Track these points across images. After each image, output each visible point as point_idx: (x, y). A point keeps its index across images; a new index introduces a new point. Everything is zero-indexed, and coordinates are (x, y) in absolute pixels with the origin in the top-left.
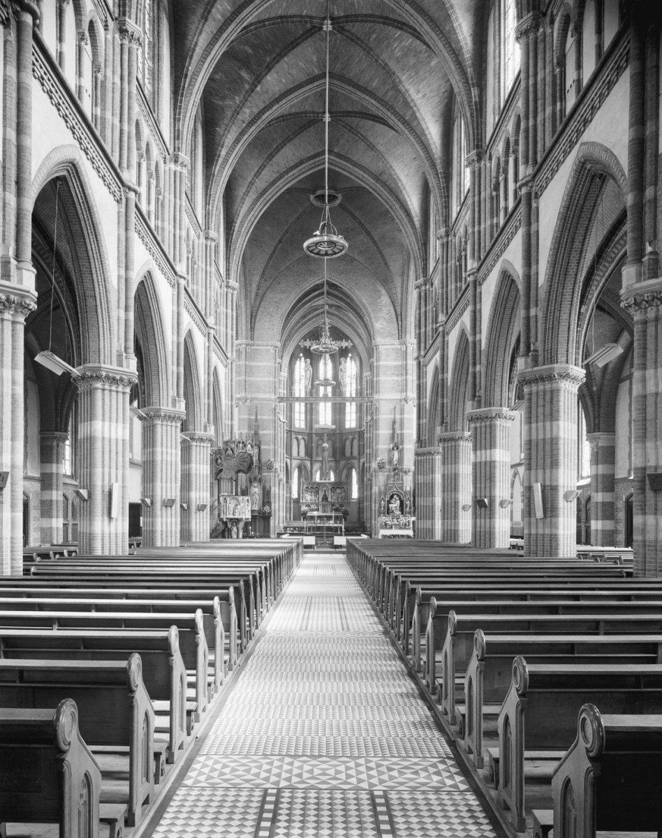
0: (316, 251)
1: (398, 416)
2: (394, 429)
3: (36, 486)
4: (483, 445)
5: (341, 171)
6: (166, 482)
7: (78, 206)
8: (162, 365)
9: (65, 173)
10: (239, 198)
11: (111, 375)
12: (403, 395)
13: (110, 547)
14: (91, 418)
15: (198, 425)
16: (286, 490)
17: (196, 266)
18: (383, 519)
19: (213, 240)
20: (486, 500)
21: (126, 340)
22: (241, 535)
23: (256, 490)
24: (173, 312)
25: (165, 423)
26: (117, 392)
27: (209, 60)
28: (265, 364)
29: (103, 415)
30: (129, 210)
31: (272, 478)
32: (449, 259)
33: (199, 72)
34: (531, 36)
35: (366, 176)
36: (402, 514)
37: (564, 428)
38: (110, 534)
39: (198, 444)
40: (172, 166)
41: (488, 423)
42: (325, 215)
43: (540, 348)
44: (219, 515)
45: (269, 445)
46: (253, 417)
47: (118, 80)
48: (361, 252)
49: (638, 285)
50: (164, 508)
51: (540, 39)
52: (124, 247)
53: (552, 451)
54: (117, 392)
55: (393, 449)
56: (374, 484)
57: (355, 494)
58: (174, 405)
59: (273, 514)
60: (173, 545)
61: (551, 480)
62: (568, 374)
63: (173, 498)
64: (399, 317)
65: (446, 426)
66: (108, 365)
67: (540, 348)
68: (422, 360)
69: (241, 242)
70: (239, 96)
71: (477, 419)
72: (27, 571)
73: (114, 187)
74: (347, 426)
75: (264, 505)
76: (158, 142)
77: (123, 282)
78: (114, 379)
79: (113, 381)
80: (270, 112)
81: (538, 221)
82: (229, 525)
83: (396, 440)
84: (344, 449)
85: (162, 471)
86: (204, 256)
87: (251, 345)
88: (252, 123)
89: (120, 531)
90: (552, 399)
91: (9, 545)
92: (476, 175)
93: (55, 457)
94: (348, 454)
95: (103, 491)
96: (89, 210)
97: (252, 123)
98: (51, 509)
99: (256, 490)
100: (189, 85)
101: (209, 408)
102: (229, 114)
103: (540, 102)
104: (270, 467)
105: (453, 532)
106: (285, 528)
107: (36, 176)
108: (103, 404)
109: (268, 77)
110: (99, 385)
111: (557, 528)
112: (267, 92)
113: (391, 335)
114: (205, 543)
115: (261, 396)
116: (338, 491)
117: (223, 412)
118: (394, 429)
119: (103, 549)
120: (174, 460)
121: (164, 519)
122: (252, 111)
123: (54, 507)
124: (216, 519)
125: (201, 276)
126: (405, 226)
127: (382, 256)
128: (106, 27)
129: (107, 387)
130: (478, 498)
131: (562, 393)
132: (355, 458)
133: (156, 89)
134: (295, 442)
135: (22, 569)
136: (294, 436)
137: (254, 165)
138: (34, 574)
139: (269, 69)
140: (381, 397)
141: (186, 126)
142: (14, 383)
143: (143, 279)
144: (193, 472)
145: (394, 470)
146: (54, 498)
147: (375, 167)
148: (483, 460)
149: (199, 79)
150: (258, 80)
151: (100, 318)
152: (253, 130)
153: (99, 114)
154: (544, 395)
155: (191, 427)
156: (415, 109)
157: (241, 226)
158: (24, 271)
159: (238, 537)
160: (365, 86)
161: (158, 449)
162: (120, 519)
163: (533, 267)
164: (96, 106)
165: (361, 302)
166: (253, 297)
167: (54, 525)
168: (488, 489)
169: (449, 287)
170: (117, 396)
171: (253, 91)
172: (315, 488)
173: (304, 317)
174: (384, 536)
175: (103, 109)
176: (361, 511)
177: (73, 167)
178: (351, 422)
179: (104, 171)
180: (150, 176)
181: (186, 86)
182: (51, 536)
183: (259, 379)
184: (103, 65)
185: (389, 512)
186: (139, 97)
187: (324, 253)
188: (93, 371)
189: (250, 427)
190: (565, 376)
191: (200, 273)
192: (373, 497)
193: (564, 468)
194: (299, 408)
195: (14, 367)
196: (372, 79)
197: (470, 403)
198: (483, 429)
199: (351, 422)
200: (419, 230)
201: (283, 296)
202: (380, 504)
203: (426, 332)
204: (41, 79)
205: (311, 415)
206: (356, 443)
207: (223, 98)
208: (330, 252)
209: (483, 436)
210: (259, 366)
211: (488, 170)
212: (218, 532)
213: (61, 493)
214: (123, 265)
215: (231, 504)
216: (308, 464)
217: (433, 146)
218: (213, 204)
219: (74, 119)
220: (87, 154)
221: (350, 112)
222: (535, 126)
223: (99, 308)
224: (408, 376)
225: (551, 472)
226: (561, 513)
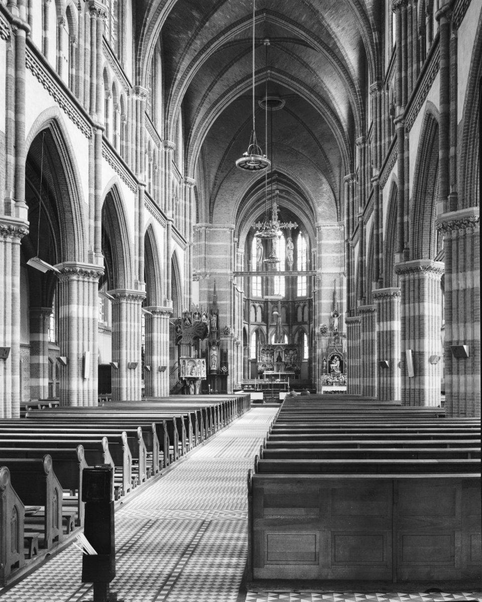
0: (246, 167)
1: (338, 288)
2: (334, 299)
3: (27, 352)
4: (385, 318)
5: (281, 84)
6: (130, 349)
7: (58, 148)
8: (126, 255)
9: (49, 126)
10: (195, 108)
11: (84, 270)
13: (84, 401)
14: (69, 302)
15: (158, 300)
16: (242, 355)
17: (157, 170)
18: (325, 377)
19: (171, 148)
20: (387, 362)
21: (95, 243)
22: (197, 392)
23: (215, 353)
24: (135, 212)
25: (129, 302)
26: (89, 282)
27: (163, 11)
28: (221, 243)
29: (78, 300)
30: (97, 144)
31: (229, 342)
32: (366, 162)
33: (156, 21)
34: (403, 9)
35: (302, 88)
36: (342, 372)
37: (429, 309)
38: (83, 391)
39: (159, 316)
40: (135, 97)
41: (388, 300)
42: (252, 138)
43: (410, 247)
44: (179, 375)
45: (226, 313)
46: (212, 290)
47: (88, 46)
48: (305, 146)
49: (444, 215)
50: (129, 370)
51: (409, 11)
52: (93, 172)
53: (419, 326)
54: (89, 282)
55: (334, 316)
56: (317, 347)
58: (136, 287)
59: (229, 373)
60: (137, 400)
61: (419, 348)
62: (430, 267)
63: (136, 362)
64: (338, 202)
65: (365, 300)
66: (82, 262)
67: (410, 247)
68: (350, 242)
69: (196, 146)
70: (191, 31)
71: (380, 296)
72: (22, 416)
73: (86, 128)
74: (299, 295)
75: (221, 366)
76: (122, 80)
77: (93, 198)
78: (86, 272)
79: (86, 274)
80: (217, 42)
81: (408, 150)
82: (188, 384)
83: (336, 309)
84: (296, 315)
85: (127, 340)
86: (164, 161)
87: (210, 227)
88: (203, 50)
89: (91, 389)
90: (419, 285)
91: (10, 398)
92: (378, 101)
93: (41, 328)
94: (300, 319)
95: (78, 358)
96: (67, 149)
97: (203, 50)
98: (39, 371)
99: (215, 353)
100: (148, 31)
102: (183, 45)
103: (409, 60)
104: (226, 332)
105: (371, 388)
106: (243, 386)
107: (28, 137)
108: (78, 292)
109: (215, 15)
110: (75, 277)
111: (423, 384)
112: (214, 27)
113: (331, 218)
115: (219, 271)
116: (291, 352)
117: (183, 288)
118: (334, 299)
119: (78, 402)
120: (136, 331)
121: (129, 378)
122: (202, 42)
123: (41, 369)
124: (177, 379)
125: (161, 178)
126: (336, 130)
127: (322, 150)
128: (79, 8)
129: (81, 279)
130: (382, 361)
131: (426, 282)
132: (305, 323)
133: (121, 39)
134: (252, 309)
135: (19, 415)
136: (251, 304)
137: (207, 81)
138: (27, 418)
139: (215, 9)
141: (145, 64)
142: (13, 285)
143: (110, 190)
144: (155, 339)
145: (335, 334)
146: (41, 362)
147: (309, 81)
148: (385, 330)
149: (156, 27)
150: (206, 18)
151: (75, 227)
152: (204, 57)
153: (74, 73)
154: (414, 282)
155: (153, 302)
156: (336, 39)
157: (197, 131)
158: (20, 208)
159: (195, 393)
160: (295, 20)
161: (124, 323)
162: (91, 379)
163: (406, 185)
164: (72, 67)
165: (305, 189)
166: (211, 186)
167: (41, 384)
168: (389, 354)
169: (366, 185)
170: (89, 285)
171: (202, 27)
172: (270, 350)
173: (258, 200)
174: (326, 392)
175: (78, 70)
176: (310, 369)
177: (55, 121)
178: (302, 291)
179: (78, 118)
180: (116, 107)
181: (145, 33)
182: (39, 393)
183: (217, 257)
184: (77, 37)
185: (330, 371)
186: (106, 51)
187: (253, 168)
188: (70, 267)
189: (209, 299)
190: (429, 269)
191: (160, 175)
192: (317, 357)
193: (429, 338)
194: (256, 281)
195: (13, 274)
196: (301, 15)
197: (375, 283)
198: (385, 305)
200: (347, 134)
201: (238, 185)
202: (323, 364)
203: (353, 219)
204: (32, 68)
205: (267, 285)
206: (306, 309)
207: (178, 33)
208: (257, 167)
209: (385, 310)
210: (217, 246)
211: (386, 97)
212: (178, 389)
213: (46, 357)
214: (93, 186)
215: (189, 366)
216: (264, 328)
217: (351, 70)
218: (171, 119)
219: (56, 88)
220: (65, 109)
221: (285, 38)
222: (406, 77)
223: (75, 220)
225: (419, 342)
226: (427, 372)
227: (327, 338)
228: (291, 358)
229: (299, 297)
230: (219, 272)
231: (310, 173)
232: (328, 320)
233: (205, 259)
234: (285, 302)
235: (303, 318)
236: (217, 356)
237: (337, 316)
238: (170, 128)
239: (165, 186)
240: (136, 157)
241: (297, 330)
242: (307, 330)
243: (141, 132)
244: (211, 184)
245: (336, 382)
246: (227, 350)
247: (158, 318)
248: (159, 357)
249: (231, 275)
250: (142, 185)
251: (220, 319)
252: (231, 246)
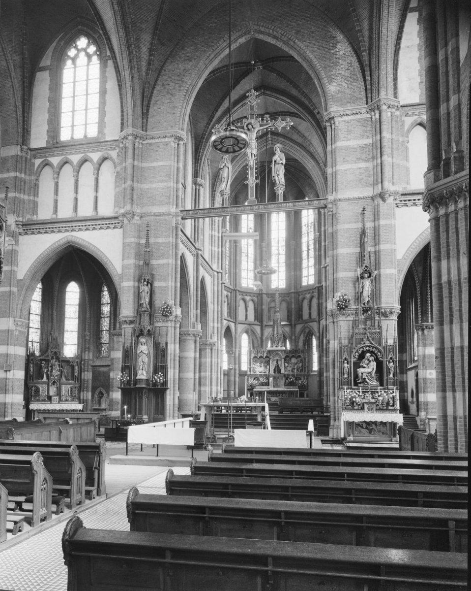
1: (369, 225)
2: (362, 245)
12: (378, 189)
18: (347, 393)
28: (160, 163)
45: (166, 280)
46: (143, 241)
57: (315, 367)
64: (367, 69)
74: (304, 283)
75: (155, 372)
83: (367, 262)
94: (306, 316)
101: (175, 290)
113: (353, 100)
115: (156, 209)
116: (294, 360)
118: (362, 245)
132: (314, 321)
134: (242, 303)
136: (239, 297)
140: (341, 195)
145: (365, 311)
165: (304, 58)
166: (144, 69)
174: (350, 425)
176: (321, 384)
183: (154, 186)
185: (357, 381)
189: (138, 256)
199: (308, 278)
201: (189, 65)
202: (342, 368)
210: (154, 168)
224: (385, 158)
227: (351, 318)
228: (293, 369)
229: (305, 286)
231: (313, 29)
232: (351, 285)
233: (133, 189)
234: (285, 295)
235: (310, 314)
236: (148, 355)
237: (370, 276)
241: (302, 331)
242: (316, 330)
244: (144, 64)
245: (369, 403)
246: (167, 343)
249: (176, 216)
250: (198, 249)
251: (156, 290)
252: (178, 169)
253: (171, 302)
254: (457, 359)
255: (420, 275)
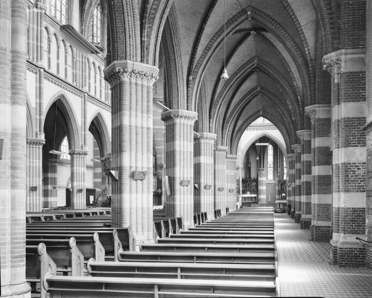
25: (31, 146)
39: (78, 156)
40: (35, 10)
50: (31, 191)
75: (158, 189)
114: (84, 210)
218: (85, 25)
230: (156, 128)
238: (85, 32)
239: (82, 70)
240: (37, 49)
243: (40, 33)
246: (162, 178)
247: (77, 157)
248: (78, 183)
253: (163, 163)
254: (210, 205)
255: (259, 149)
